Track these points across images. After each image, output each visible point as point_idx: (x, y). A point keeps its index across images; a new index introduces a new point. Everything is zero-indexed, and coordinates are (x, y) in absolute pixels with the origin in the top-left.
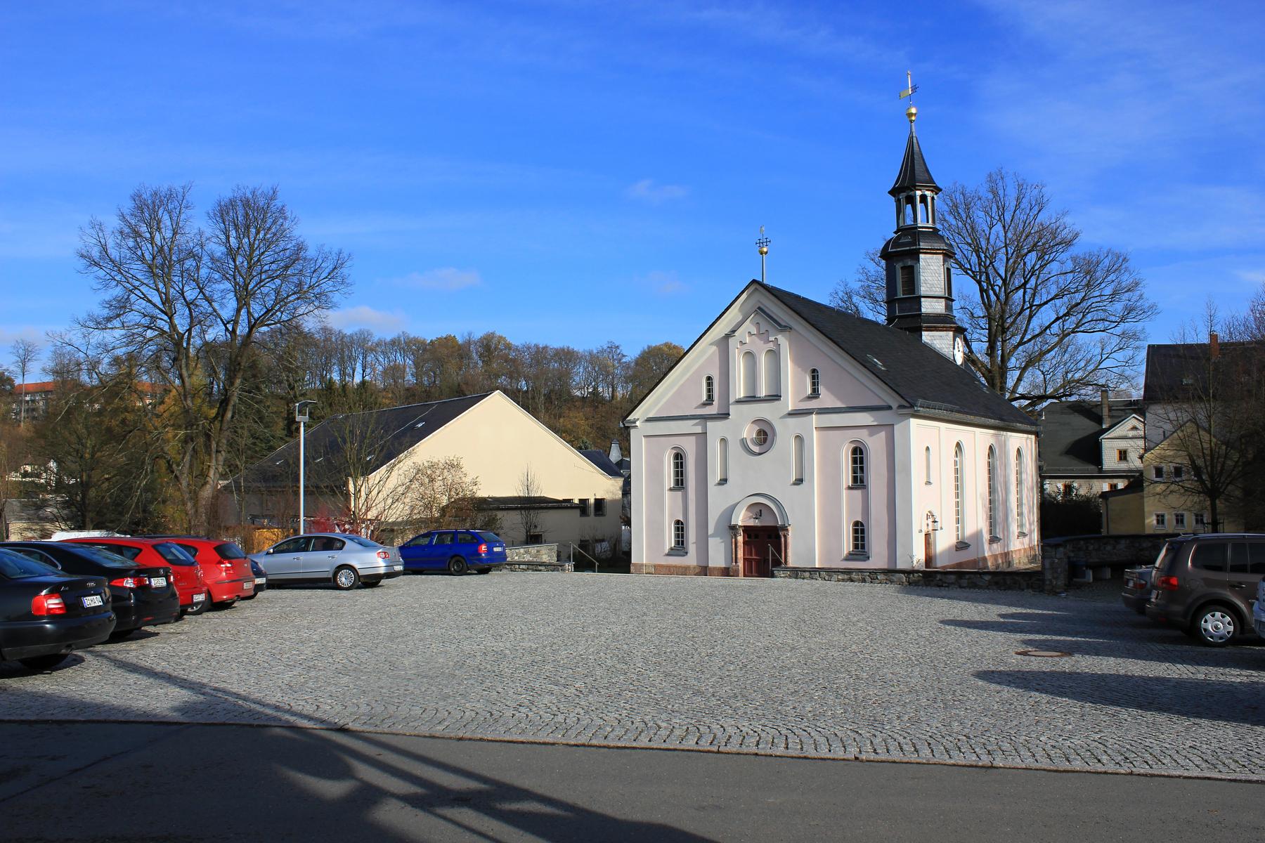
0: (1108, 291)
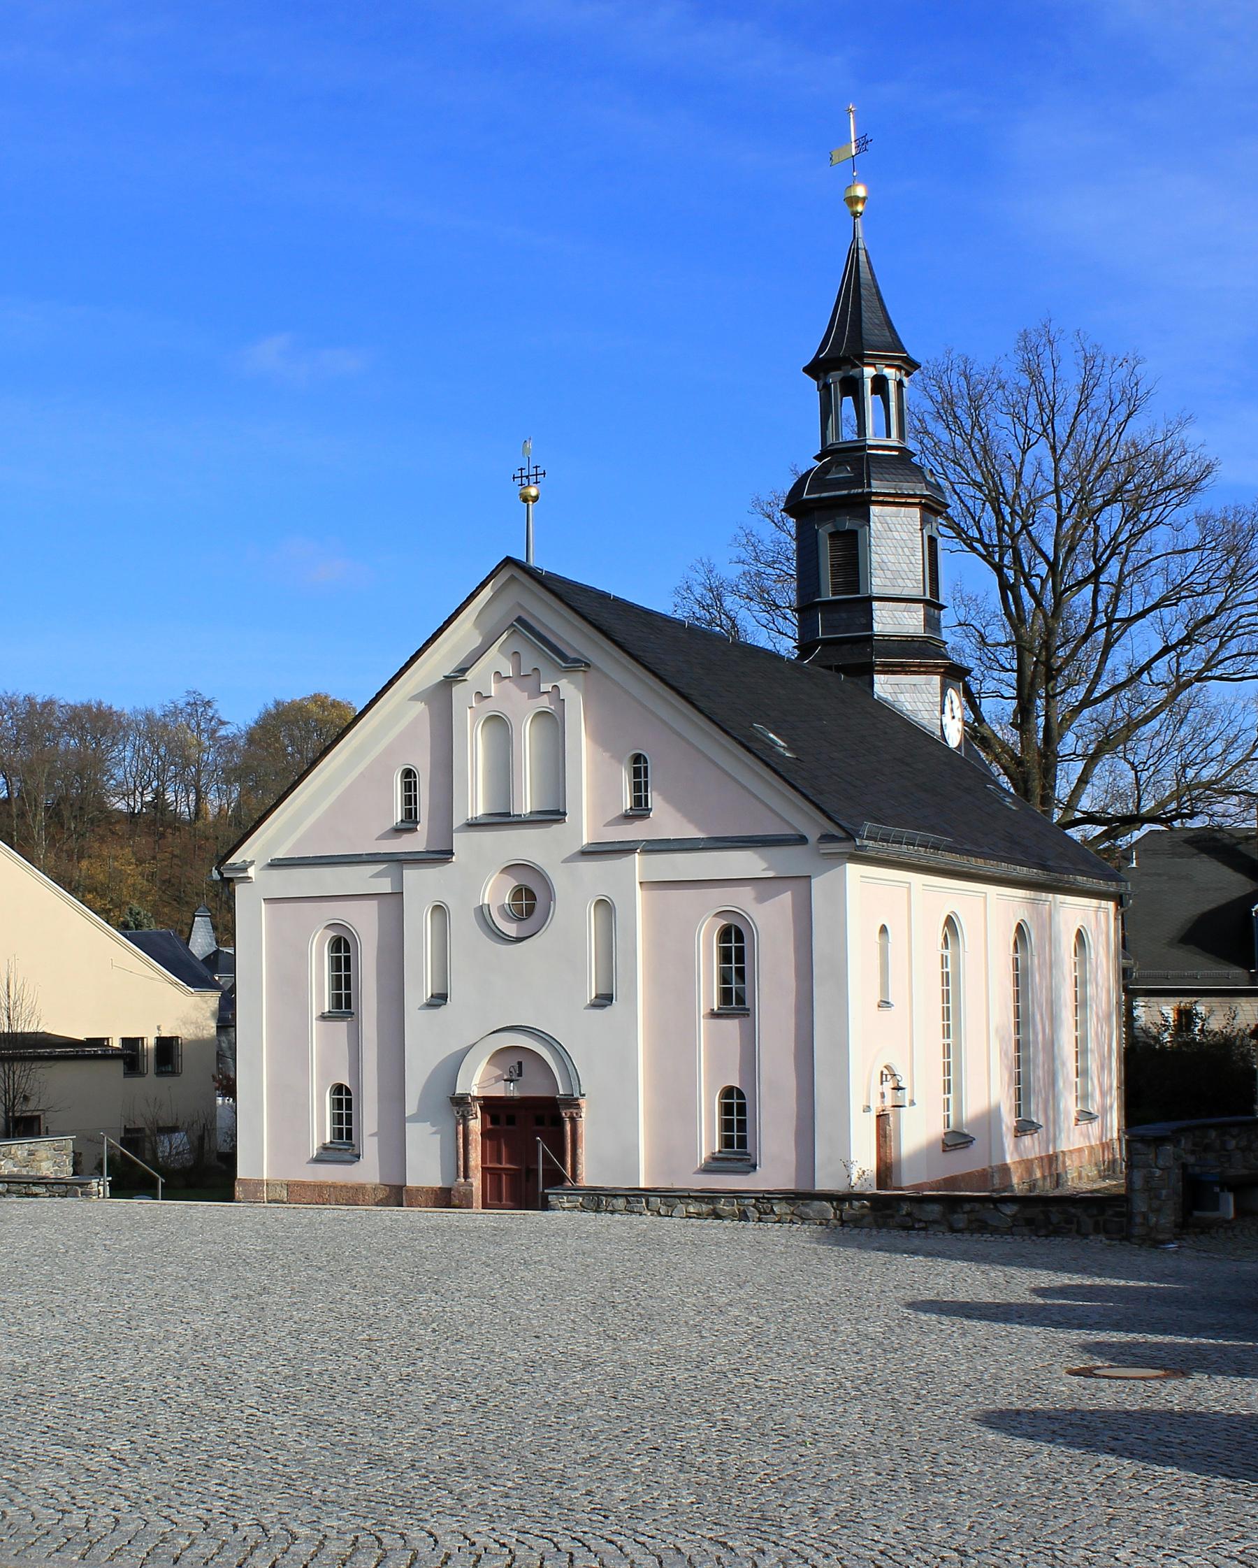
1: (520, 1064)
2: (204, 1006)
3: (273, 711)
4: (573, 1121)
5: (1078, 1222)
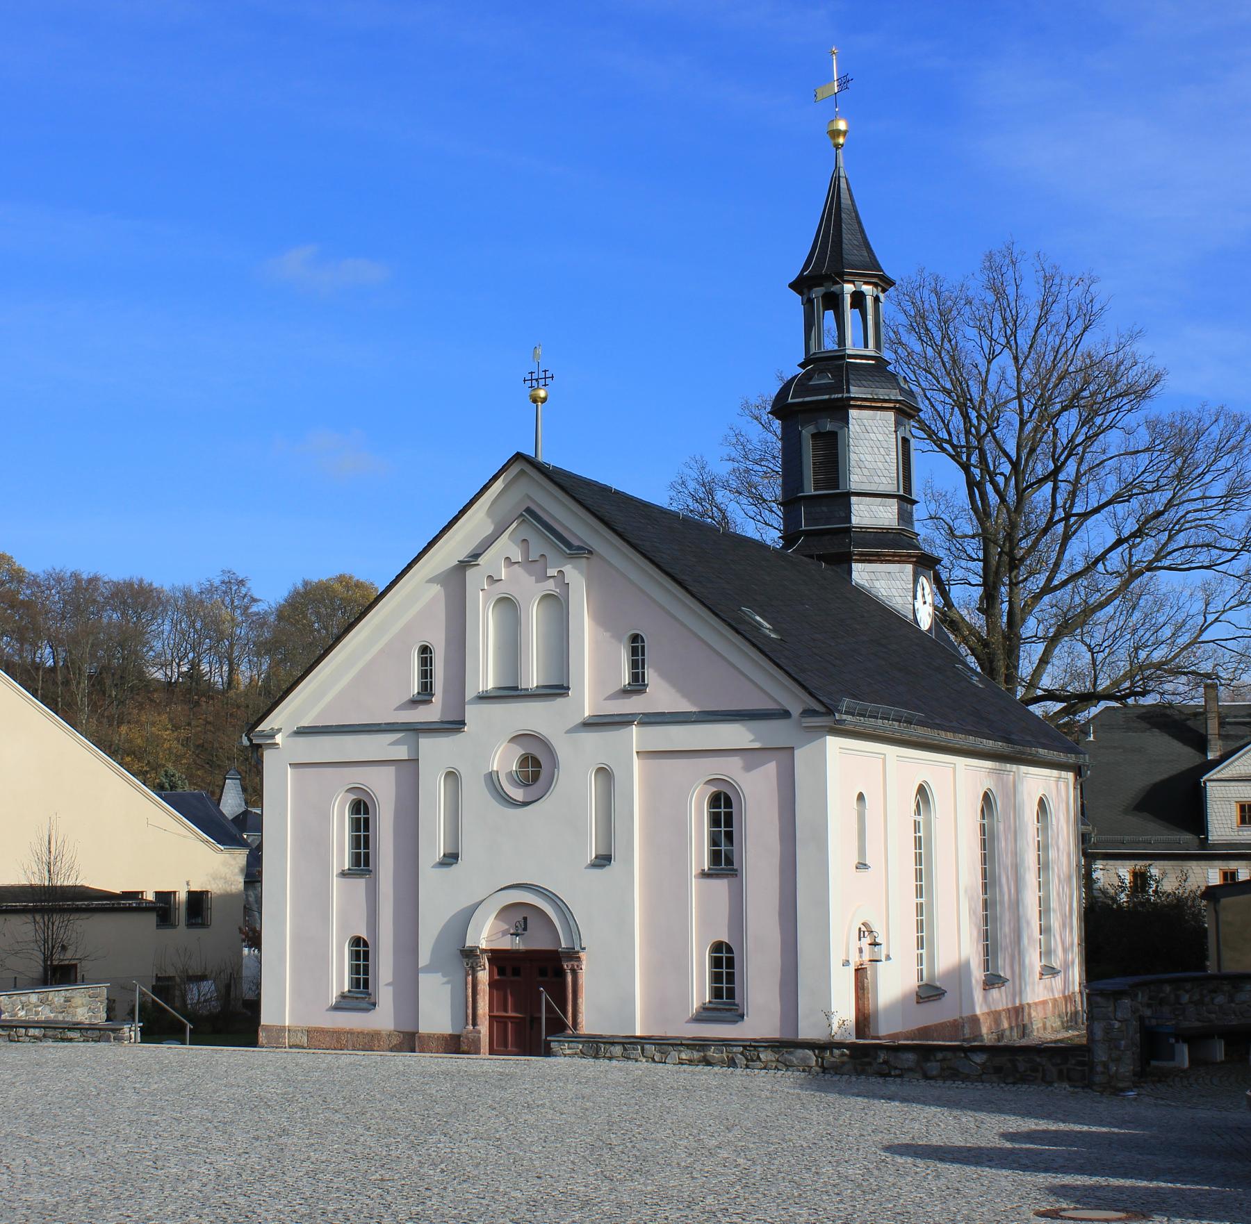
1: (525, 919)
2: (233, 862)
3: (301, 589)
4: (575, 973)
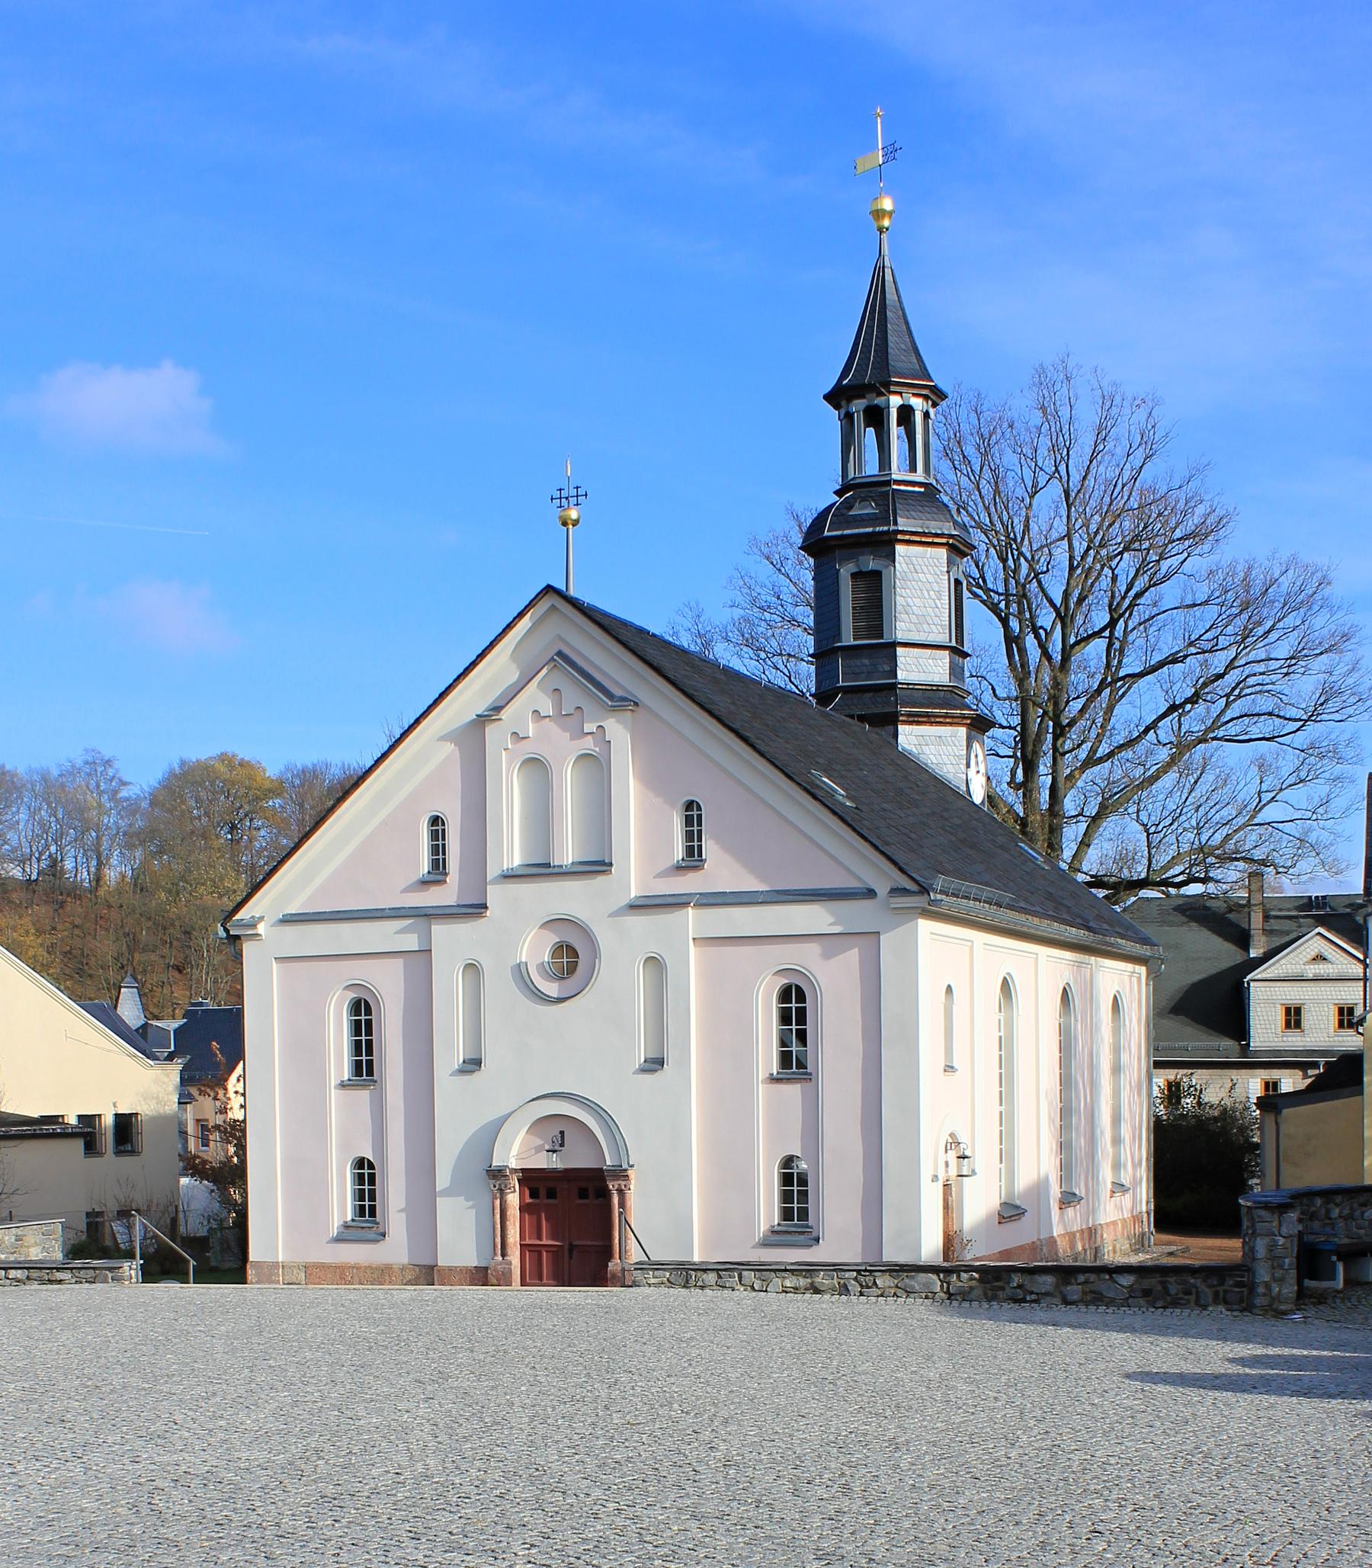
0: (1283, 650)
1: (562, 1133)
2: (166, 1080)
3: (178, 771)
4: (621, 1192)
5: (1197, 1293)
